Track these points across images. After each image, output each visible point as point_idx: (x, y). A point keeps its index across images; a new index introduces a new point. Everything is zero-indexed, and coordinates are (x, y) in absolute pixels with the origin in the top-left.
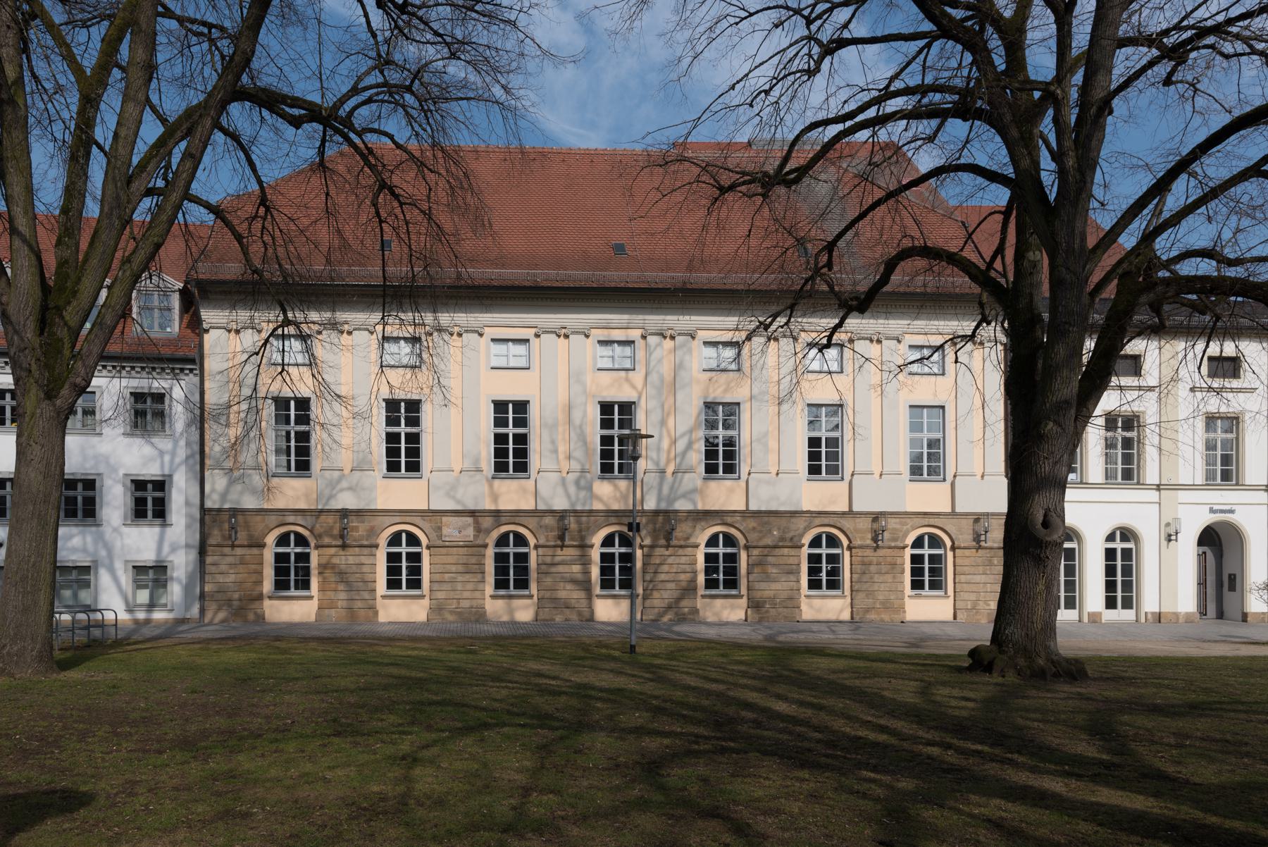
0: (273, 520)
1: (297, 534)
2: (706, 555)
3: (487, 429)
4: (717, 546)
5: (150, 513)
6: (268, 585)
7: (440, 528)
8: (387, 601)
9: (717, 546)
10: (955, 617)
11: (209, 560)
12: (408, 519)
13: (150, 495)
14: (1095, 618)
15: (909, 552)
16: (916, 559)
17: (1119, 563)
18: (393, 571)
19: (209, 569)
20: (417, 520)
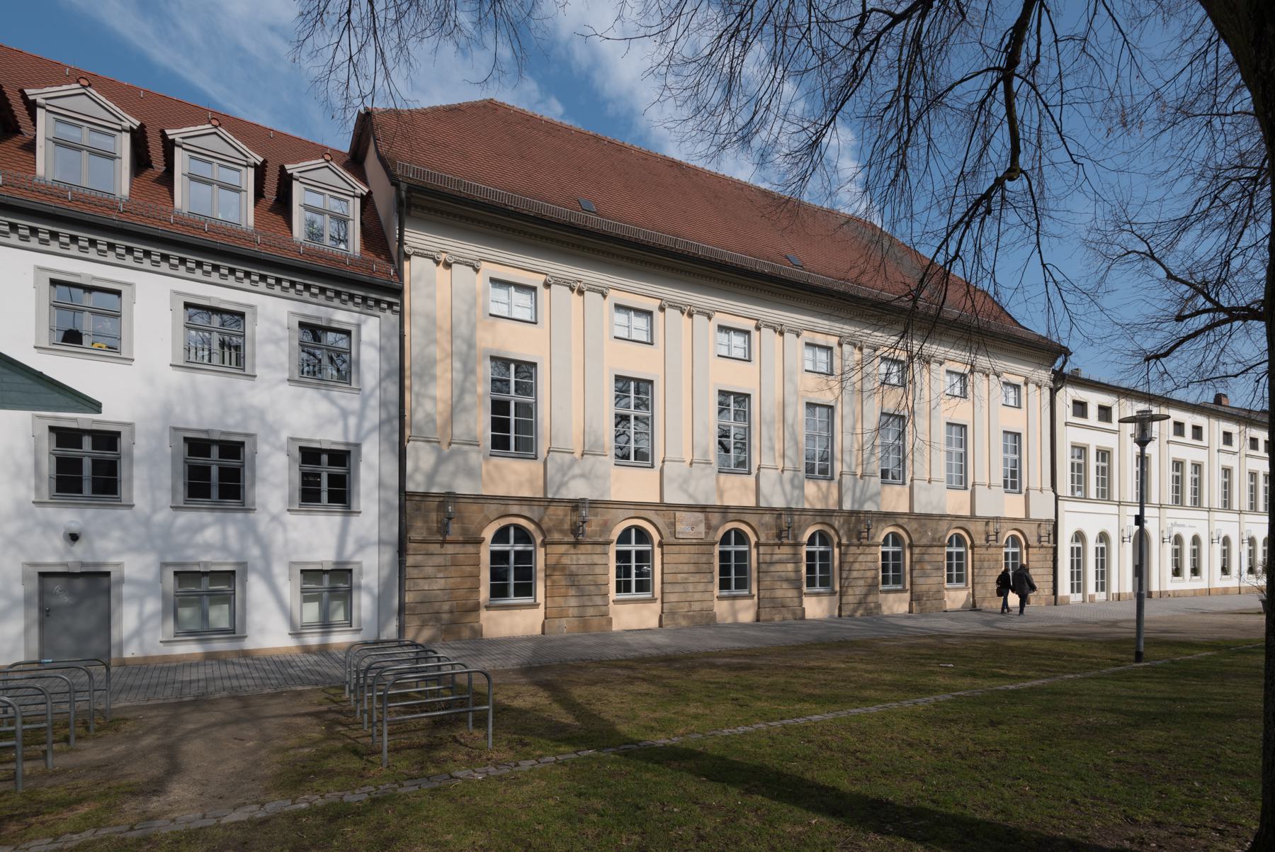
0: (493, 509)
1: (518, 528)
2: (493, 554)
3: (607, 410)
4: (629, 542)
5: (325, 496)
6: (484, 593)
7: (674, 524)
8: (619, 607)
9: (629, 542)
10: (661, 625)
11: (410, 560)
12: (642, 513)
13: (325, 471)
14: (1092, 597)
15: (717, 549)
16: (724, 556)
17: (955, 562)
18: (623, 572)
19: (410, 572)
20: (651, 515)
